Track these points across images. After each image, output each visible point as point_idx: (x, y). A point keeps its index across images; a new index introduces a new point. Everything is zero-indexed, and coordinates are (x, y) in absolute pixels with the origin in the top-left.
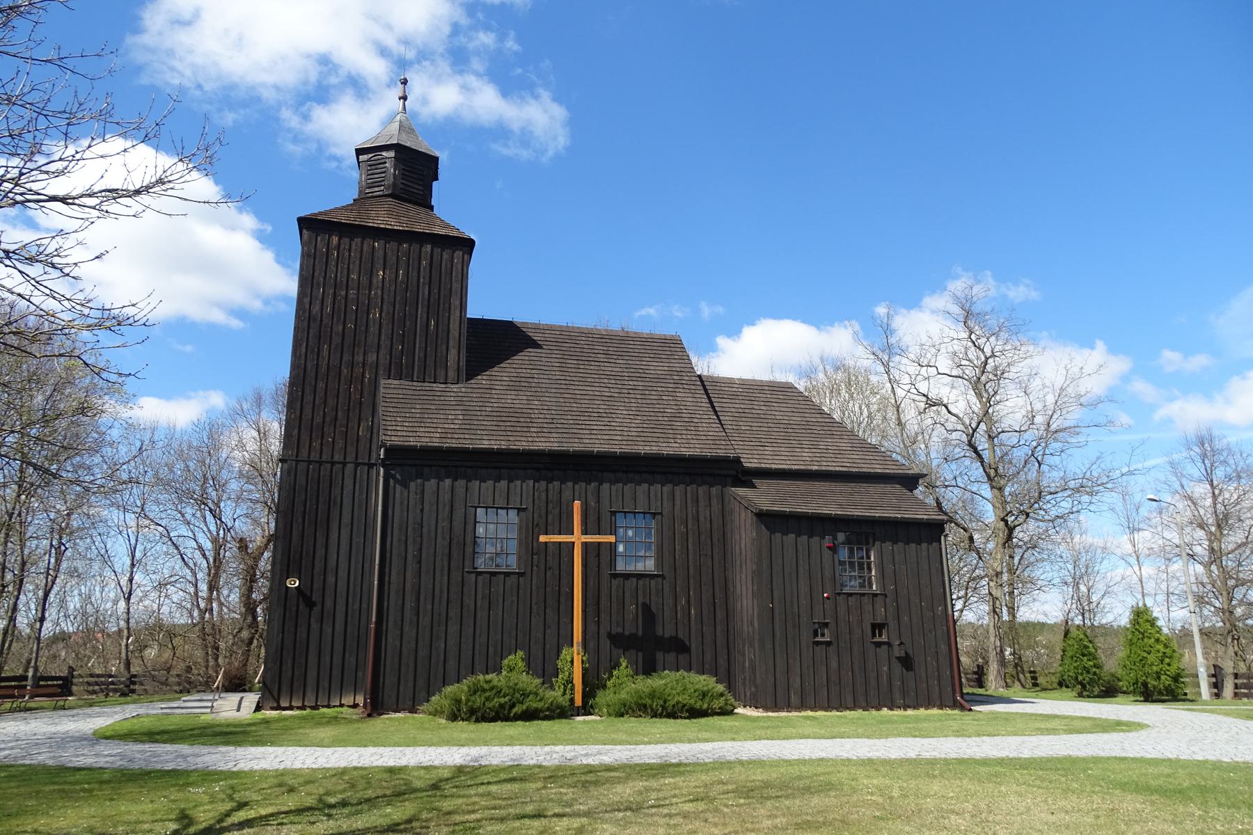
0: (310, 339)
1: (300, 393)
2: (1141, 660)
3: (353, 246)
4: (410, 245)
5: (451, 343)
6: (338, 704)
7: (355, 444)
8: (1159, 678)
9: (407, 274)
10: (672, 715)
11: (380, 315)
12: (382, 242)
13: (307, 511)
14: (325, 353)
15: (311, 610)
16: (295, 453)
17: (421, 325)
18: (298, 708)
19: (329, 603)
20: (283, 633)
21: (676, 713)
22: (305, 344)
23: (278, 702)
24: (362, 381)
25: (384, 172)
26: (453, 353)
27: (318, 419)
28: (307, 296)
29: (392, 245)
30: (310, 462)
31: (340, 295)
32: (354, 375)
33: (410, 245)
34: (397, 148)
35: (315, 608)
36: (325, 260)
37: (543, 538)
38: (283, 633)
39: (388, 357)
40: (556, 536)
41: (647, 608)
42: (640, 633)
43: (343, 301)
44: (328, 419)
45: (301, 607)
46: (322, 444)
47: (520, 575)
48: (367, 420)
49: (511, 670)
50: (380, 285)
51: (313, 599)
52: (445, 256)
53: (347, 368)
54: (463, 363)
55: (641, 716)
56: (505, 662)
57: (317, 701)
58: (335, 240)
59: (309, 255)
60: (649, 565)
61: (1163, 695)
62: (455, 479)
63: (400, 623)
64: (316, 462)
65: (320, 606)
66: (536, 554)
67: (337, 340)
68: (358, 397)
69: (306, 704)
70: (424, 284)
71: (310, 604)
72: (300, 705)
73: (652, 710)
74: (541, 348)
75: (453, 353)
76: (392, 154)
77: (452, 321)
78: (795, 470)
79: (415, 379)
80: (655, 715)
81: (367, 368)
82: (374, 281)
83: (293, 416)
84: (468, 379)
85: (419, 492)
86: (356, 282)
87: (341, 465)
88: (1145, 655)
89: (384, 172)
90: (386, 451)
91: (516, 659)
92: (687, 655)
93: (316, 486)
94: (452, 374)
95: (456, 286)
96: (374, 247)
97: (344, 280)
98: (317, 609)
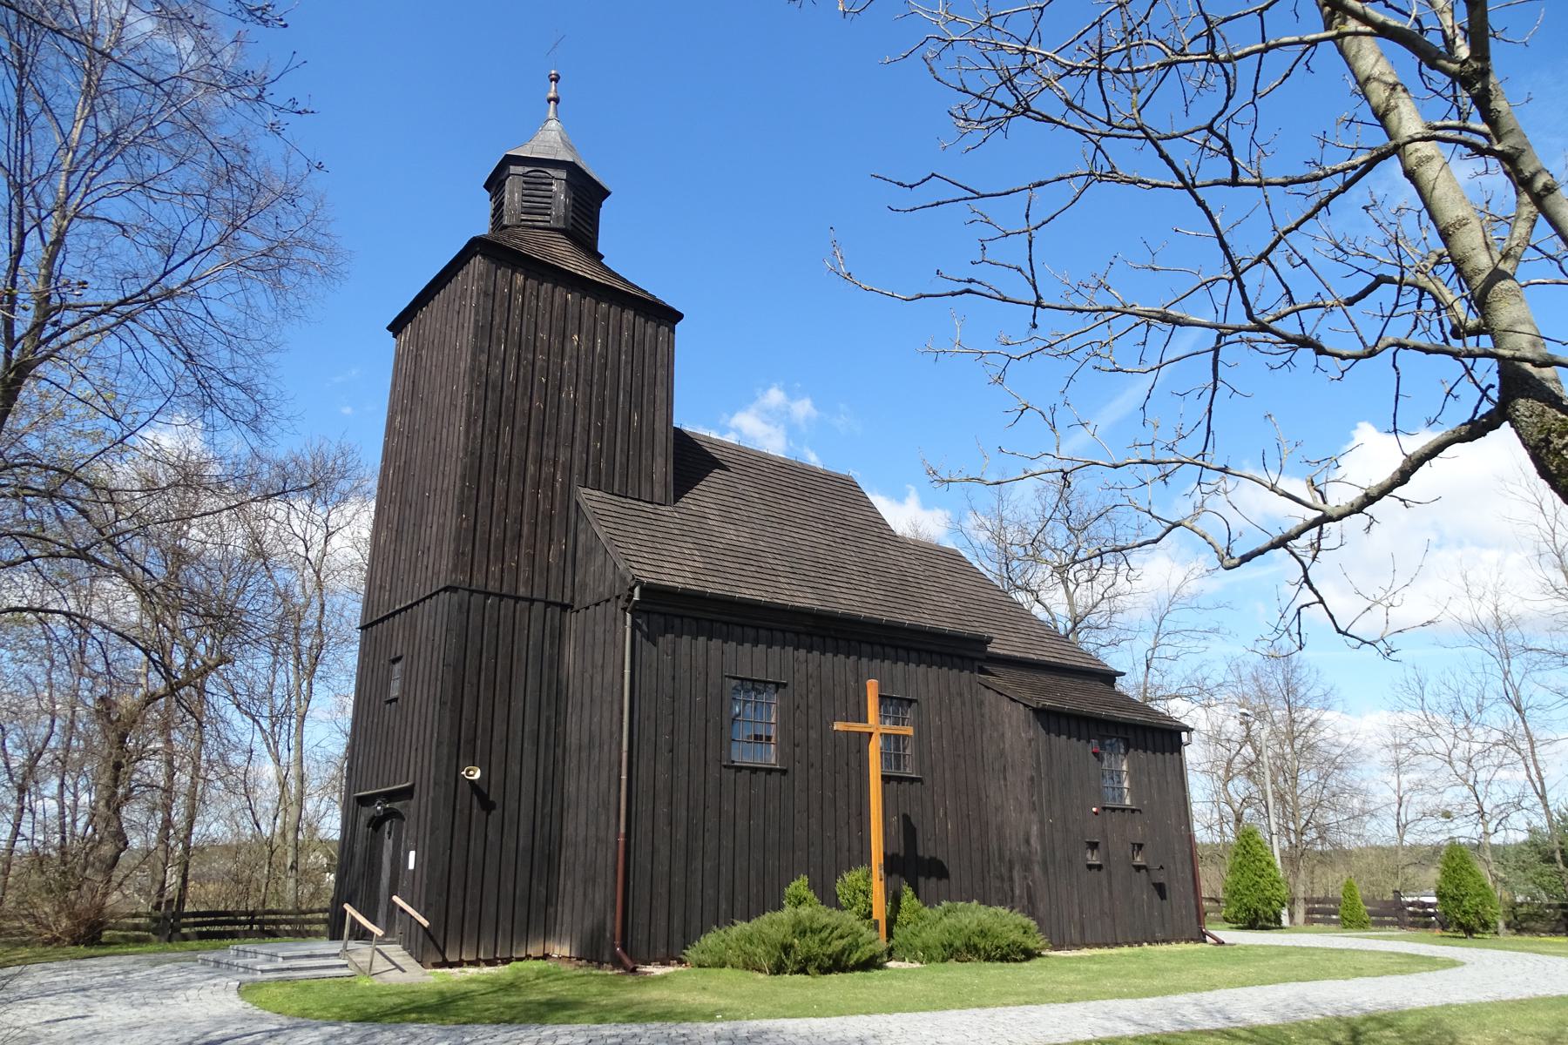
0: (488, 416)
1: (475, 492)
2: (1254, 885)
3: (542, 293)
4: (610, 307)
5: (657, 450)
6: (524, 955)
7: (545, 575)
8: (1270, 904)
9: (605, 345)
10: (1004, 958)
11: (575, 396)
12: (577, 295)
13: (483, 666)
14: (506, 438)
15: (488, 814)
16: (467, 579)
17: (623, 418)
18: (470, 963)
19: (512, 805)
20: (451, 849)
21: (1008, 955)
22: (481, 421)
23: (443, 954)
24: (553, 486)
25: (550, 197)
26: (660, 461)
27: (497, 533)
28: (483, 352)
29: (588, 302)
30: (487, 594)
31: (526, 359)
32: (543, 476)
33: (610, 307)
34: (572, 168)
35: (493, 812)
36: (506, 305)
37: (838, 726)
38: (451, 849)
39: (584, 456)
40: (855, 724)
41: (906, 818)
42: (902, 854)
43: (530, 368)
44: (509, 534)
45: (475, 811)
46: (502, 570)
47: (784, 772)
48: (560, 541)
49: (800, 903)
50: (575, 353)
51: (491, 799)
52: (650, 331)
53: (535, 465)
54: (670, 478)
55: (970, 960)
56: (789, 891)
57: (495, 952)
58: (519, 279)
59: (486, 294)
60: (770, 756)
61: (1271, 922)
62: (710, 639)
63: (651, 835)
64: (495, 595)
65: (500, 810)
66: (798, 746)
67: (520, 422)
68: (548, 507)
69: (464, 957)
70: (626, 362)
71: (487, 806)
72: (474, 958)
73: (986, 951)
74: (729, 471)
75: (660, 461)
76: (563, 175)
77: (657, 418)
78: (1004, 655)
79: (603, 487)
80: (988, 959)
81: (560, 467)
82: (568, 349)
83: (464, 524)
84: (675, 502)
85: (669, 652)
86: (546, 343)
87: (527, 604)
88: (1257, 879)
89: (550, 197)
90: (642, 590)
91: (800, 886)
92: (946, 881)
93: (494, 631)
94: (659, 492)
95: (661, 373)
96: (567, 300)
97: (532, 338)
98: (496, 813)
